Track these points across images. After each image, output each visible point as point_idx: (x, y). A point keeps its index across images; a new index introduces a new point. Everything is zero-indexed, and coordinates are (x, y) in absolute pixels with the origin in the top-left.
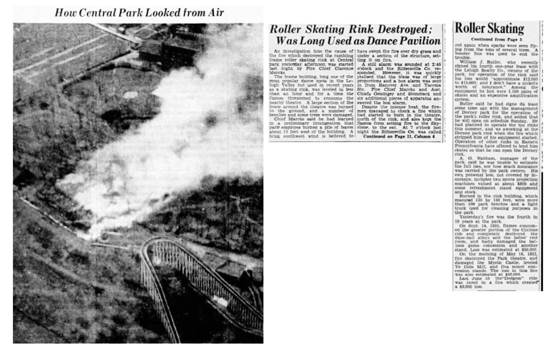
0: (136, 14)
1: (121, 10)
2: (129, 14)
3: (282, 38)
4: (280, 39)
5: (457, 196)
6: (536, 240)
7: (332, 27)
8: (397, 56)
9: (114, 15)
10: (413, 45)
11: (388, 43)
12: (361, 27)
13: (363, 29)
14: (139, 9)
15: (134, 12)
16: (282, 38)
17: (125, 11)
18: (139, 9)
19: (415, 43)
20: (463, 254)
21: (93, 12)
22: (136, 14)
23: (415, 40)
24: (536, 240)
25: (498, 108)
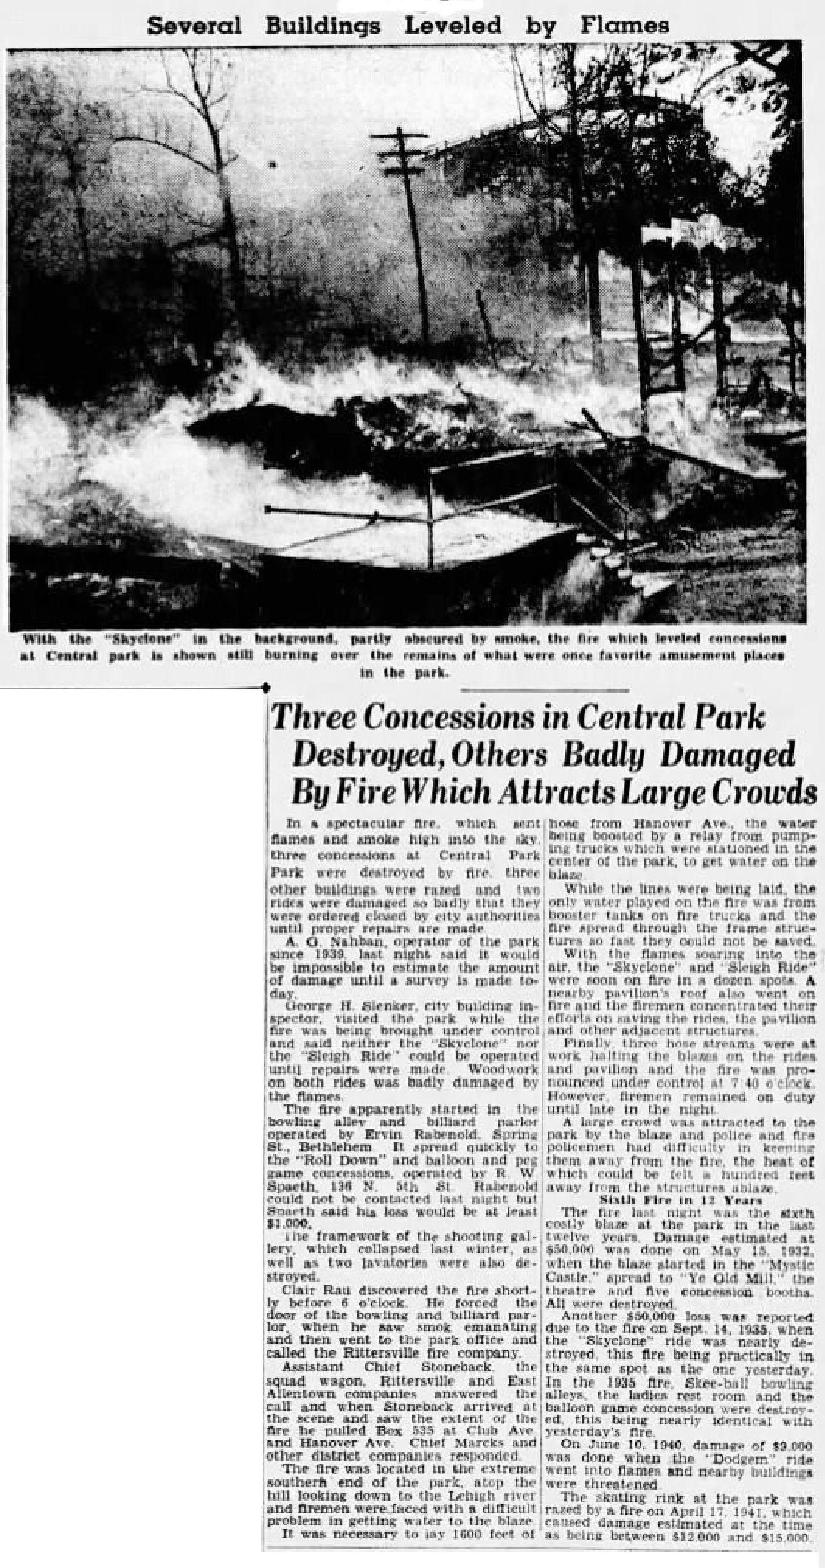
0: (745, 721)
1: (701, 706)
2: (725, 721)
3: (417, 780)
4: (412, 784)
5: (277, 1471)
6: (808, 1338)
7: (551, 711)
8: (605, 862)
9: (680, 726)
10: (575, 804)
11: (579, 801)
12: (551, 711)
13: (557, 715)
14: (753, 705)
15: (739, 715)
16: (417, 780)
17: (713, 710)
18: (753, 705)
19: (579, 801)
20: (572, 1444)
21: (619, 715)
22: (745, 721)
23: (777, 789)
24: (808, 1338)
25: (667, 1097)
